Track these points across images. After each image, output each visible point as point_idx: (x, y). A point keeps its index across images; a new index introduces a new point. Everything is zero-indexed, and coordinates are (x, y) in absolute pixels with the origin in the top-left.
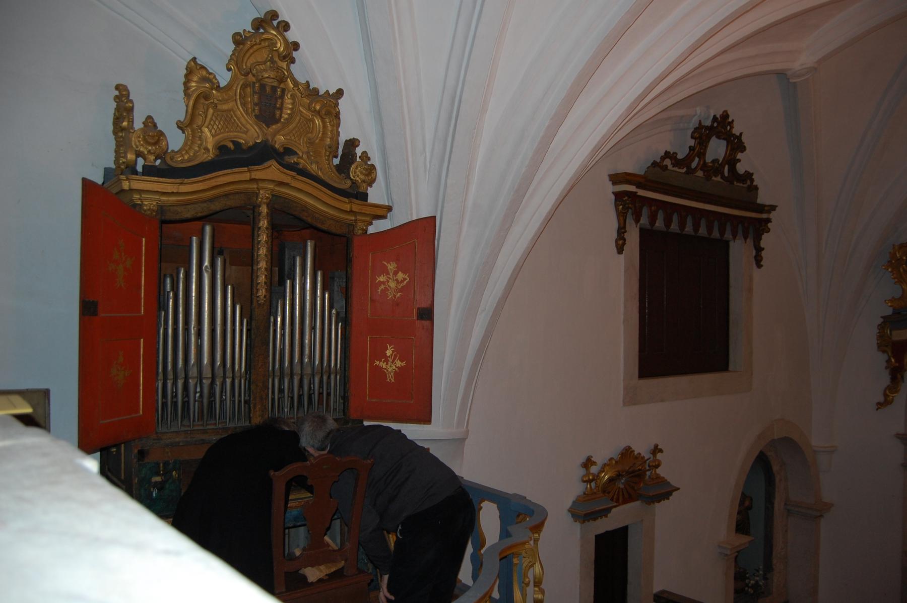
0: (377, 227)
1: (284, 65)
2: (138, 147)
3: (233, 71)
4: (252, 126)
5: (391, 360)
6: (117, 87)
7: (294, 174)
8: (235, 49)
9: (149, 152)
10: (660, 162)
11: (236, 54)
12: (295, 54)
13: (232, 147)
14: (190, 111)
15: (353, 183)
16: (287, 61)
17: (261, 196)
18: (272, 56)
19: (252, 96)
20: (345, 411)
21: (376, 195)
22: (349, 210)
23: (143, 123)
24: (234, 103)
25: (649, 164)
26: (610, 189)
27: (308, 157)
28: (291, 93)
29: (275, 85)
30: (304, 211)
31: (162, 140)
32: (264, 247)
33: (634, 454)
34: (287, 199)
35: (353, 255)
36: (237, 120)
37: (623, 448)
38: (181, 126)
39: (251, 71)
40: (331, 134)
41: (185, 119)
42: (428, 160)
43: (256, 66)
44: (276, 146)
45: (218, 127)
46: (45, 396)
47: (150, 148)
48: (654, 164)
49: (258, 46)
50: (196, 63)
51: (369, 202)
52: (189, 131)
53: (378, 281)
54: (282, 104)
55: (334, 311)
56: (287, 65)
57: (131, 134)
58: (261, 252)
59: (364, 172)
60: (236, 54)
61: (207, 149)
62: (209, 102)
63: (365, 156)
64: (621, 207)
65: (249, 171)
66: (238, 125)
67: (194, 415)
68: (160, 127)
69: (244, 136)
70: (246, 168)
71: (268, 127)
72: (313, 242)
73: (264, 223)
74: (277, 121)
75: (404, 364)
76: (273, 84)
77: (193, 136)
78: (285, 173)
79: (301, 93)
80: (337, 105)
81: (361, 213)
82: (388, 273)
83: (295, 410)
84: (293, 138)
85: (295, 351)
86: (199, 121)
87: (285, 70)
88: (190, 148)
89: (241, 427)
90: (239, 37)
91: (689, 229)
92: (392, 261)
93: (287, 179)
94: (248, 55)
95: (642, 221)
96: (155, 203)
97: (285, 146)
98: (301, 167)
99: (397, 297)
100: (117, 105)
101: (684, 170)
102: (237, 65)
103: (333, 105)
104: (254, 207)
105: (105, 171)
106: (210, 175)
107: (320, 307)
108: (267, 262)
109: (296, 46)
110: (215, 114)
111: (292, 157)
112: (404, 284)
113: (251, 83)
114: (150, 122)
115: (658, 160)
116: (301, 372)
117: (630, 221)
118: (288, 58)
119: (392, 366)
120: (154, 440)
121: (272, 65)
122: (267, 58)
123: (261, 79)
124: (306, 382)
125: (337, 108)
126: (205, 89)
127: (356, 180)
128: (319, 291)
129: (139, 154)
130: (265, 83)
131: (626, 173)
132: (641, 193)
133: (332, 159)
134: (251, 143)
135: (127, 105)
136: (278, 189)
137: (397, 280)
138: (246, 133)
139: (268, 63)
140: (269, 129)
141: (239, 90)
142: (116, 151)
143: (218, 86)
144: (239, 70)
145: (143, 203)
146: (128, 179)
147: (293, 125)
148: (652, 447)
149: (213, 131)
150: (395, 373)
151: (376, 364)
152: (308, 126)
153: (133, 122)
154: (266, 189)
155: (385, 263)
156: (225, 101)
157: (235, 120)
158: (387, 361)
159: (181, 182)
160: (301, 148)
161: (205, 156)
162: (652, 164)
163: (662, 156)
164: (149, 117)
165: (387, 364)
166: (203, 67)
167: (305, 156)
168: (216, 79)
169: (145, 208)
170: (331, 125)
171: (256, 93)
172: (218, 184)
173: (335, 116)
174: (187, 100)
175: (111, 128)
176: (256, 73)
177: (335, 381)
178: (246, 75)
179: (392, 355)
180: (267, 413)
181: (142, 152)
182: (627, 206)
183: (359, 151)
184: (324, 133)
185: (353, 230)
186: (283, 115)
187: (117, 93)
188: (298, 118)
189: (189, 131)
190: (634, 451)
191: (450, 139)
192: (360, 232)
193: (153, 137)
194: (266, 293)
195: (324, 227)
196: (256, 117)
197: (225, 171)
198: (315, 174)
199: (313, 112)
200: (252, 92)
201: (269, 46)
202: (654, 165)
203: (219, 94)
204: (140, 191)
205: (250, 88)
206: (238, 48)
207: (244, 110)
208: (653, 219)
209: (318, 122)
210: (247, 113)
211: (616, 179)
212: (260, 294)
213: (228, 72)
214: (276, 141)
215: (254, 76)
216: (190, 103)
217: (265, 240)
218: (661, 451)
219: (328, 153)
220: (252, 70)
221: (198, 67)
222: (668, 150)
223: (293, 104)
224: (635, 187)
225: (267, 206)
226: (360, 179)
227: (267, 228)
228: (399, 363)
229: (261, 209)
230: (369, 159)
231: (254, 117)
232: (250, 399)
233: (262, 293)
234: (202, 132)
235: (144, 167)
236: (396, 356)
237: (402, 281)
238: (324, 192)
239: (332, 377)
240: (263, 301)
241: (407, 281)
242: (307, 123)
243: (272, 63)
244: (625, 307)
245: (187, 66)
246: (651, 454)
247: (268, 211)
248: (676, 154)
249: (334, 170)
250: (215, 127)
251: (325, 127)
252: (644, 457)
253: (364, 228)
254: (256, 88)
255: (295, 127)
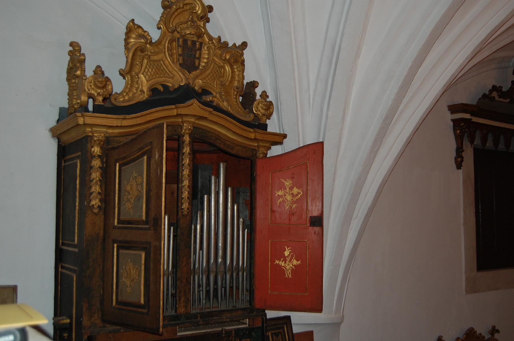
0: (275, 151)
1: (202, 23)
2: (89, 91)
3: (163, 29)
4: (177, 73)
5: (288, 259)
6: (71, 44)
7: (211, 110)
8: (164, 12)
9: (99, 94)
10: (489, 94)
11: (165, 16)
12: (210, 15)
13: (162, 89)
14: (130, 61)
15: (255, 116)
16: (204, 21)
17: (185, 128)
18: (192, 17)
19: (177, 49)
20: (251, 301)
21: (273, 126)
22: (253, 138)
23: (94, 72)
24: (163, 55)
25: (480, 96)
26: (449, 116)
27: (220, 96)
28: (207, 46)
29: (195, 40)
30: (217, 139)
31: (109, 84)
32: (187, 168)
33: (476, 334)
34: (205, 130)
35: (256, 174)
36: (165, 68)
37: (467, 329)
38: (122, 74)
39: (176, 30)
40: (238, 77)
41: (126, 68)
42: (311, 97)
43: (180, 25)
44: (196, 88)
45: (151, 74)
46: (14, 292)
47: (99, 91)
48: (484, 96)
49: (182, 10)
50: (134, 23)
51: (268, 131)
52: (128, 77)
53: (276, 195)
54: (200, 54)
55: (241, 220)
56: (203, 24)
57: (84, 80)
58: (184, 173)
59: (264, 107)
60: (165, 16)
61: (142, 91)
62: (144, 54)
63: (264, 95)
64: (459, 131)
65: (176, 108)
66: (166, 71)
67: (170, 310)
68: (106, 75)
69: (170, 80)
70: (174, 106)
71: (190, 73)
72: (225, 164)
73: (187, 150)
74: (197, 68)
75: (299, 262)
76: (193, 39)
77: (132, 81)
78: (204, 109)
79: (215, 46)
80: (242, 54)
81: (263, 140)
82: (285, 189)
83: (211, 301)
84: (208, 81)
85: (211, 253)
86: (136, 69)
87: (202, 27)
88: (130, 90)
89: (169, 316)
90: (167, 3)
91: (502, 147)
92: (288, 179)
93: (206, 115)
94: (174, 16)
95: (475, 143)
96: (102, 135)
97: (202, 88)
98: (215, 104)
99: (293, 207)
100: (70, 59)
101: (508, 100)
102: (165, 24)
103: (239, 55)
104: (179, 137)
105: (60, 110)
106: (146, 112)
107: (230, 217)
108: (189, 181)
109: (210, 9)
110: (148, 63)
111: (208, 96)
112: (299, 197)
113: (176, 38)
114: (99, 71)
115: (487, 93)
116: (216, 270)
117: (466, 143)
118: (204, 19)
119: (290, 264)
120: (100, 327)
121: (192, 24)
122: (188, 19)
123: (184, 35)
124: (219, 278)
125: (242, 57)
126: (141, 44)
127: (258, 114)
128: (229, 203)
129: (90, 96)
130: (186, 38)
131: (462, 104)
132: (475, 119)
133: (239, 97)
134: (176, 86)
135: (80, 58)
136: (198, 122)
137: (292, 194)
138: (172, 78)
139: (189, 22)
140: (190, 75)
141: (167, 44)
142: (69, 94)
143: (151, 42)
144: (167, 29)
145: (93, 135)
146: (83, 116)
147: (209, 71)
148: (491, 328)
149: (147, 77)
150: (292, 270)
151: (276, 263)
152: (220, 72)
153: (84, 71)
154: (189, 122)
155: (283, 180)
156: (156, 53)
157: (164, 68)
158: (285, 260)
159: (124, 117)
160: (215, 88)
161: (141, 96)
162: (483, 96)
163: (490, 90)
164: (99, 67)
165: (285, 263)
166: (139, 27)
167: (218, 96)
168: (150, 36)
169: (95, 139)
170: (238, 71)
171: (180, 46)
172: (152, 119)
173: (241, 63)
174: (127, 52)
175: (65, 76)
176: (180, 30)
177: (243, 276)
178: (173, 32)
179: (289, 255)
180: (190, 304)
181: (93, 94)
182: (464, 130)
183: (258, 91)
184: (233, 77)
185: (256, 154)
186: (201, 63)
187: (71, 49)
188: (212, 66)
189: (128, 77)
190: (476, 332)
191: (330, 80)
192: (261, 155)
193: (101, 82)
194: (189, 206)
195: (234, 152)
196: (180, 64)
197: (158, 108)
198: (226, 110)
199: (224, 60)
200: (177, 46)
201: (190, 9)
202: (484, 97)
203: (152, 48)
204: (91, 125)
205: (175, 43)
206: (166, 12)
207: (171, 60)
208: (484, 140)
209: (228, 68)
210: (173, 62)
211: (453, 109)
212: (184, 207)
213: (159, 30)
214: (196, 84)
215: (178, 33)
216: (129, 55)
217: (188, 163)
218: (498, 331)
219: (235, 93)
220: (177, 29)
221: (136, 27)
222: (495, 85)
223: (209, 54)
224: (470, 115)
225: (189, 136)
226: (261, 113)
227: (189, 154)
228: (295, 262)
229: (184, 138)
230: (268, 97)
231: (178, 65)
232: (176, 291)
233: (185, 206)
234: (139, 78)
235: (94, 106)
236: (292, 256)
237: (297, 195)
238: (234, 124)
239: (240, 273)
240: (186, 213)
241: (301, 194)
242: (219, 69)
243: (193, 22)
244: (464, 212)
245: (127, 26)
246: (490, 334)
247: (190, 140)
248: (502, 87)
249: (241, 106)
250: (149, 73)
251: (233, 72)
252: (484, 337)
253: (265, 152)
254: (180, 42)
255: (210, 73)
